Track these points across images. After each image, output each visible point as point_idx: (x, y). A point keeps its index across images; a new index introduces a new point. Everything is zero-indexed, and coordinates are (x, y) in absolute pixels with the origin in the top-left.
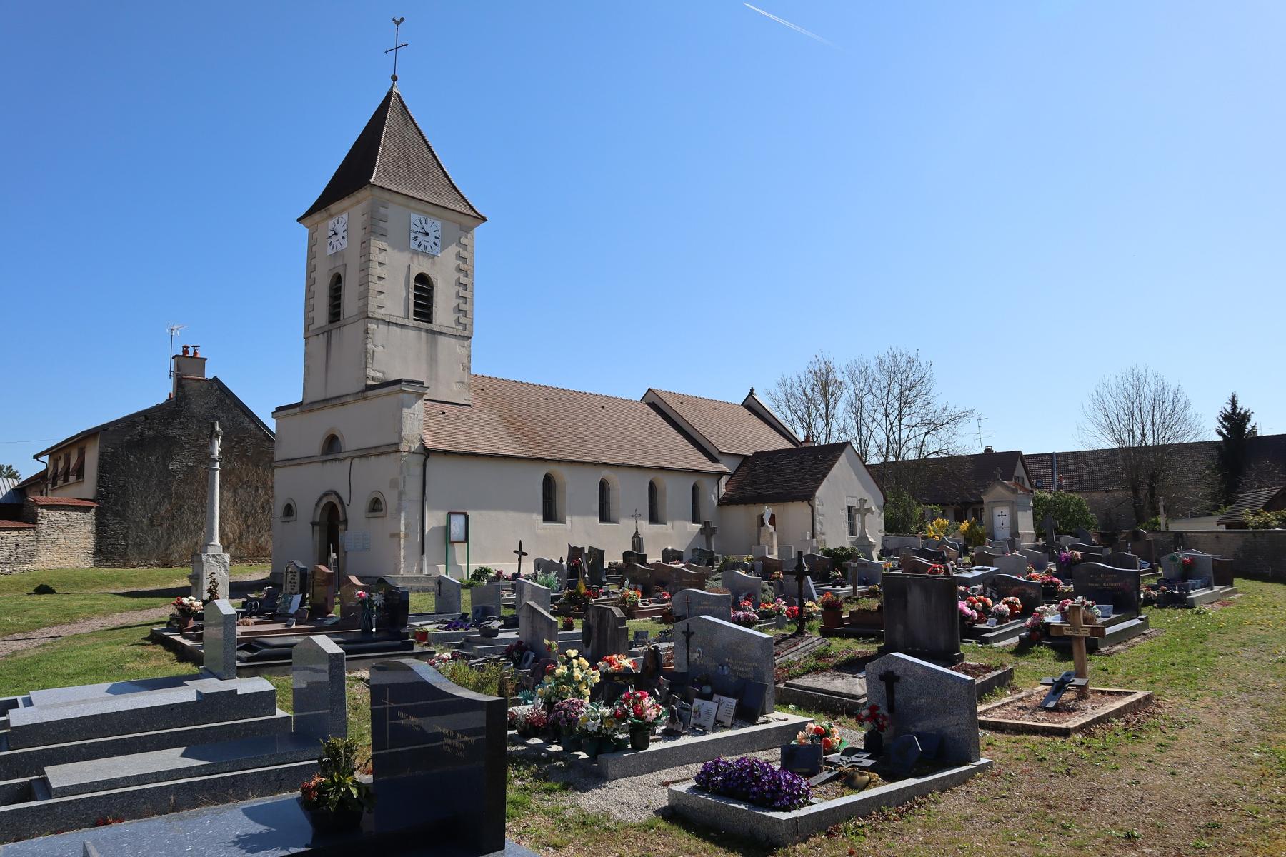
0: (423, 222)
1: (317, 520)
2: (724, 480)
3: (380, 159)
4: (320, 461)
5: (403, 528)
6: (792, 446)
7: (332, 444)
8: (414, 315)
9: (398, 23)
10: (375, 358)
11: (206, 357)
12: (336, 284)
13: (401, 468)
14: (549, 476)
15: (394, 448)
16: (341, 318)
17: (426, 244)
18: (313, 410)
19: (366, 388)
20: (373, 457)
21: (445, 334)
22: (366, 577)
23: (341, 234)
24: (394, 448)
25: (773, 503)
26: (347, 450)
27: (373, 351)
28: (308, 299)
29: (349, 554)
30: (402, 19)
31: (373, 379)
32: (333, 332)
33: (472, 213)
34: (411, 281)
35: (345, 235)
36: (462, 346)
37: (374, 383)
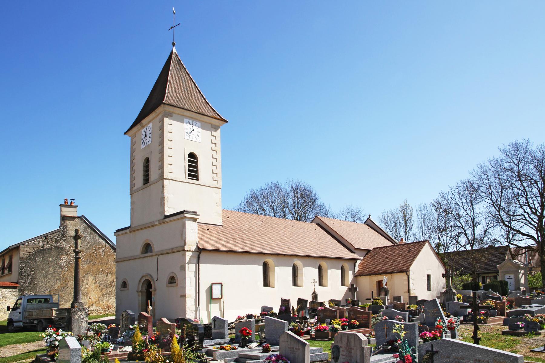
1: (140, 289)
2: (358, 262)
3: (168, 90)
6: (390, 244)
7: (147, 248)
8: (189, 176)
11: (77, 205)
12: (146, 164)
14: (266, 263)
16: (150, 181)
19: (165, 217)
23: (148, 135)
24: (182, 249)
28: (131, 175)
33: (219, 117)
35: (150, 135)
36: (216, 193)
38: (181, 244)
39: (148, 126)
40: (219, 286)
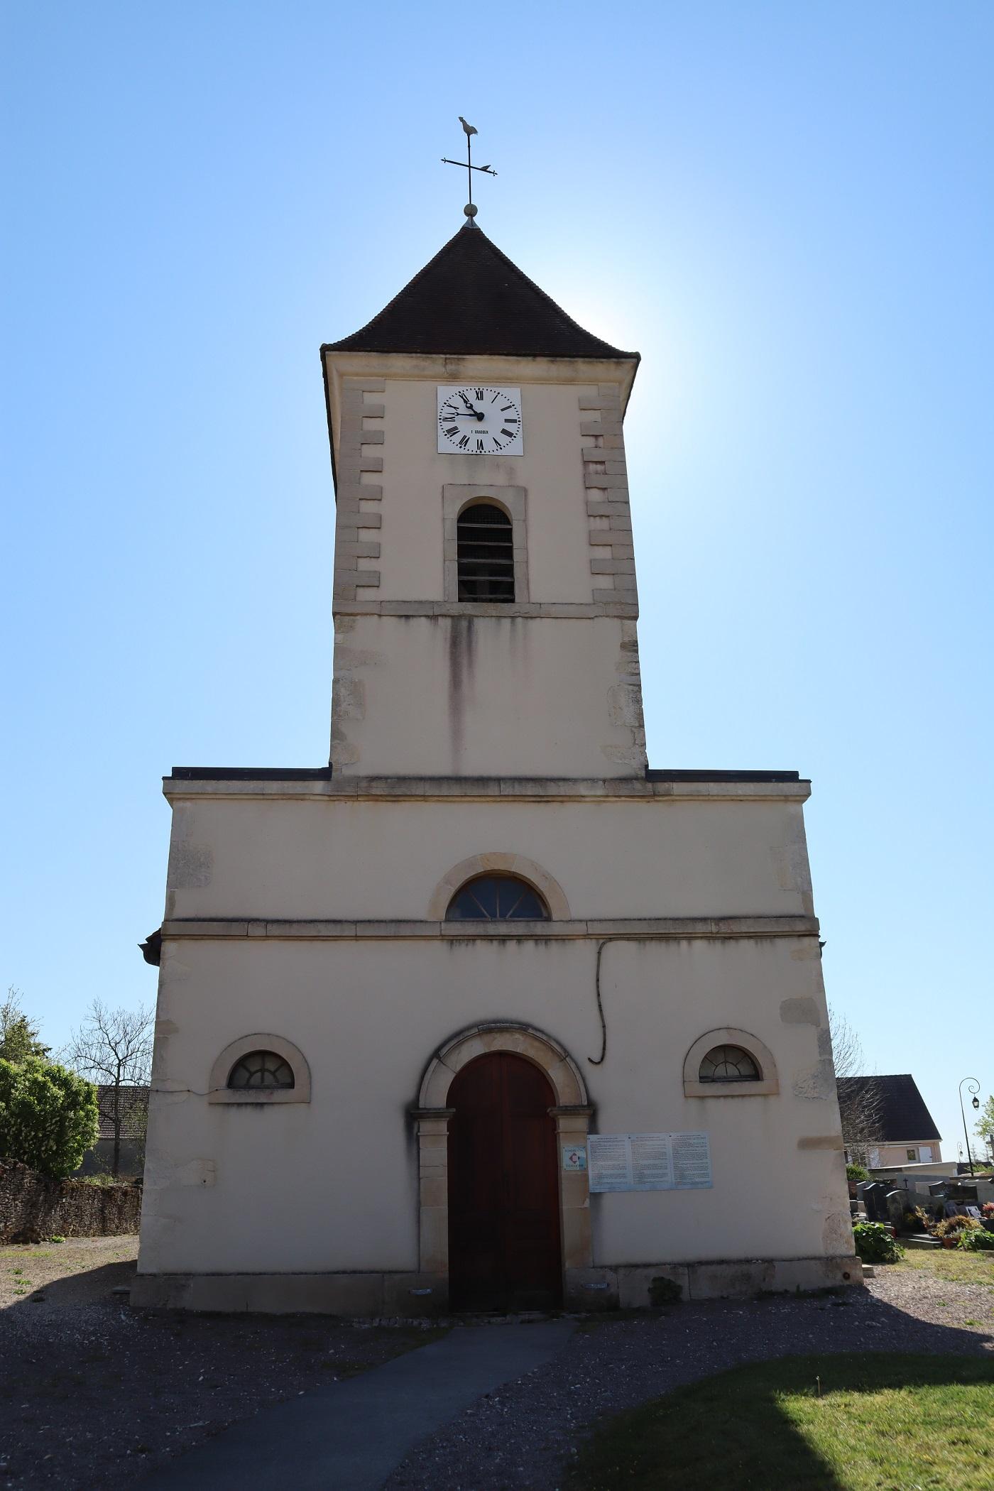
0: (471, 397)
4: (442, 937)
17: (480, 437)
22: (701, 1263)
29: (608, 1203)
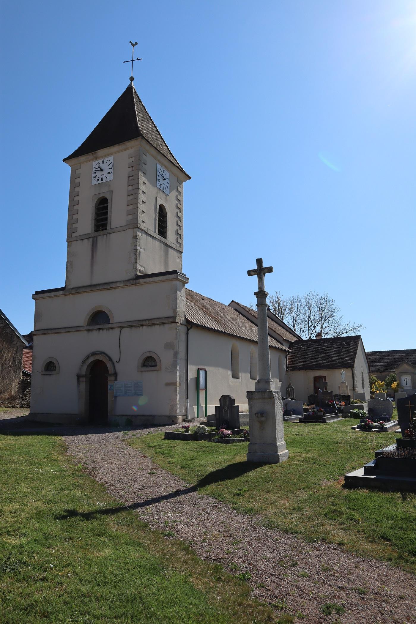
1: (84, 373)
4: (86, 330)
5: (178, 379)
6: (296, 339)
9: (133, 45)
10: (141, 257)
12: (98, 206)
13: (176, 335)
15: (172, 320)
16: (108, 227)
18: (78, 293)
20: (145, 327)
21: (172, 247)
24: (171, 320)
25: (312, 370)
26: (116, 321)
27: (140, 252)
30: (136, 43)
31: (140, 271)
32: (99, 238)
34: (157, 208)
36: (178, 258)
37: (140, 274)
38: (170, 313)
39: (108, 158)
40: (204, 372)
